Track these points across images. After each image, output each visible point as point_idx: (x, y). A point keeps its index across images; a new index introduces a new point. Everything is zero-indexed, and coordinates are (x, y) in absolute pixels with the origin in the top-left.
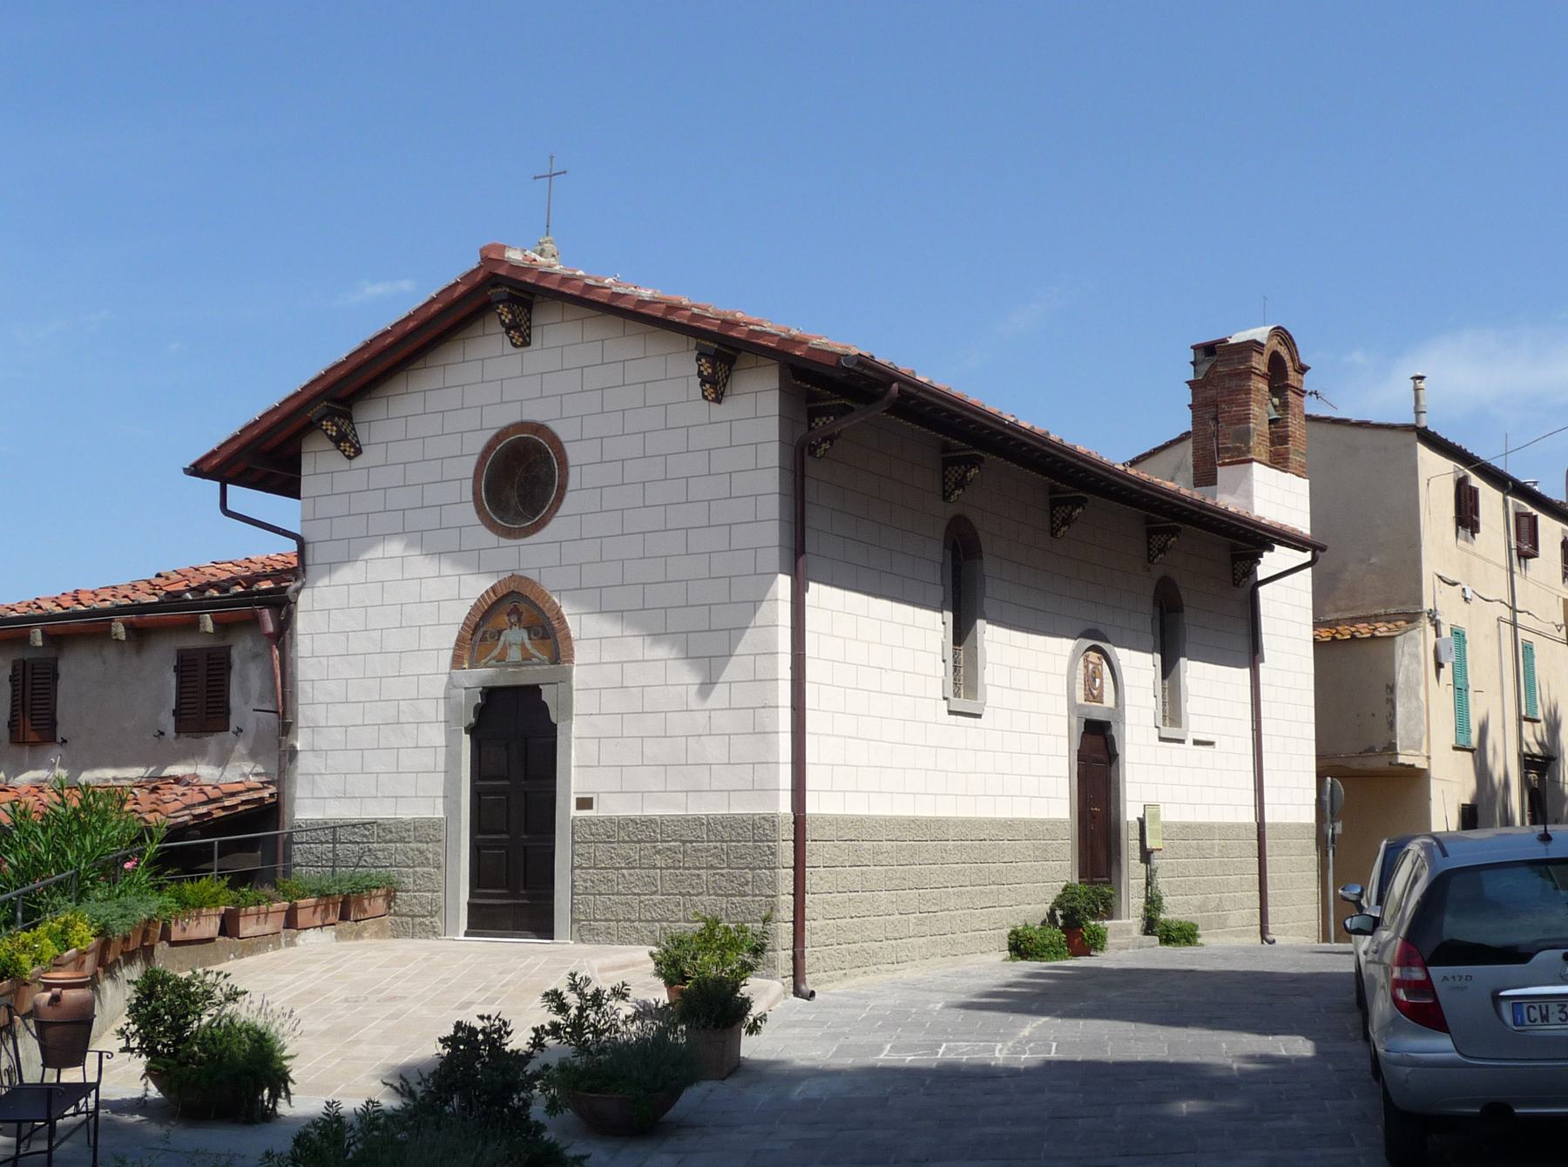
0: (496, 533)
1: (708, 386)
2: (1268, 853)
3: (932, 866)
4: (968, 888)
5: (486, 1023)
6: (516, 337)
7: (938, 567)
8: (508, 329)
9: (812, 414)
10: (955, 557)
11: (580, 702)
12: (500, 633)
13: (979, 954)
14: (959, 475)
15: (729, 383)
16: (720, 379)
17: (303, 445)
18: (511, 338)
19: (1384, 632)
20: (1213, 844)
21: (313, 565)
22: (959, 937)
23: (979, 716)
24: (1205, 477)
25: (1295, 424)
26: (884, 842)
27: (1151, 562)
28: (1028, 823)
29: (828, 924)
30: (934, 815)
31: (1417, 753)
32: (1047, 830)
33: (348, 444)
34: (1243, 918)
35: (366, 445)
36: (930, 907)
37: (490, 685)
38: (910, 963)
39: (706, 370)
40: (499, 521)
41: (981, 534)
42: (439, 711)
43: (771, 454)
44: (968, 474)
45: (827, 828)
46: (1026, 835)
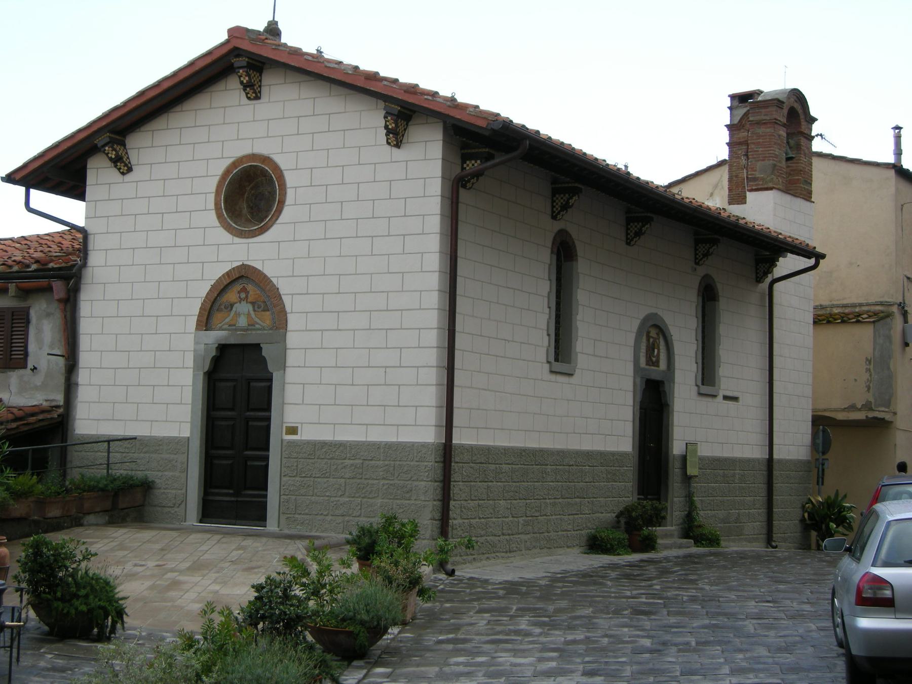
0: (231, 233)
1: (391, 135)
2: (775, 481)
3: (536, 484)
4: (560, 500)
5: (282, 577)
6: (251, 93)
7: (547, 266)
8: (245, 87)
9: (464, 158)
10: (558, 260)
11: (292, 358)
12: (232, 306)
13: (565, 548)
14: (564, 200)
15: (406, 135)
16: (401, 131)
17: (88, 162)
18: (247, 94)
19: (866, 318)
20: (734, 473)
21: (93, 250)
22: (552, 534)
23: (571, 375)
24: (737, 197)
25: (805, 162)
26: (504, 465)
27: (697, 263)
28: (602, 454)
29: (464, 523)
30: (538, 446)
31: (887, 410)
32: (617, 459)
33: (123, 165)
34: (754, 528)
35: (136, 165)
36: (533, 513)
37: (223, 342)
38: (519, 552)
39: (391, 124)
40: (234, 225)
41: (576, 242)
42: (190, 361)
43: (436, 187)
44: (570, 201)
45: (466, 454)
46: (601, 463)
